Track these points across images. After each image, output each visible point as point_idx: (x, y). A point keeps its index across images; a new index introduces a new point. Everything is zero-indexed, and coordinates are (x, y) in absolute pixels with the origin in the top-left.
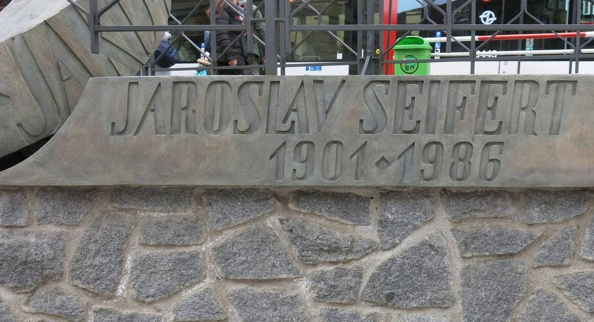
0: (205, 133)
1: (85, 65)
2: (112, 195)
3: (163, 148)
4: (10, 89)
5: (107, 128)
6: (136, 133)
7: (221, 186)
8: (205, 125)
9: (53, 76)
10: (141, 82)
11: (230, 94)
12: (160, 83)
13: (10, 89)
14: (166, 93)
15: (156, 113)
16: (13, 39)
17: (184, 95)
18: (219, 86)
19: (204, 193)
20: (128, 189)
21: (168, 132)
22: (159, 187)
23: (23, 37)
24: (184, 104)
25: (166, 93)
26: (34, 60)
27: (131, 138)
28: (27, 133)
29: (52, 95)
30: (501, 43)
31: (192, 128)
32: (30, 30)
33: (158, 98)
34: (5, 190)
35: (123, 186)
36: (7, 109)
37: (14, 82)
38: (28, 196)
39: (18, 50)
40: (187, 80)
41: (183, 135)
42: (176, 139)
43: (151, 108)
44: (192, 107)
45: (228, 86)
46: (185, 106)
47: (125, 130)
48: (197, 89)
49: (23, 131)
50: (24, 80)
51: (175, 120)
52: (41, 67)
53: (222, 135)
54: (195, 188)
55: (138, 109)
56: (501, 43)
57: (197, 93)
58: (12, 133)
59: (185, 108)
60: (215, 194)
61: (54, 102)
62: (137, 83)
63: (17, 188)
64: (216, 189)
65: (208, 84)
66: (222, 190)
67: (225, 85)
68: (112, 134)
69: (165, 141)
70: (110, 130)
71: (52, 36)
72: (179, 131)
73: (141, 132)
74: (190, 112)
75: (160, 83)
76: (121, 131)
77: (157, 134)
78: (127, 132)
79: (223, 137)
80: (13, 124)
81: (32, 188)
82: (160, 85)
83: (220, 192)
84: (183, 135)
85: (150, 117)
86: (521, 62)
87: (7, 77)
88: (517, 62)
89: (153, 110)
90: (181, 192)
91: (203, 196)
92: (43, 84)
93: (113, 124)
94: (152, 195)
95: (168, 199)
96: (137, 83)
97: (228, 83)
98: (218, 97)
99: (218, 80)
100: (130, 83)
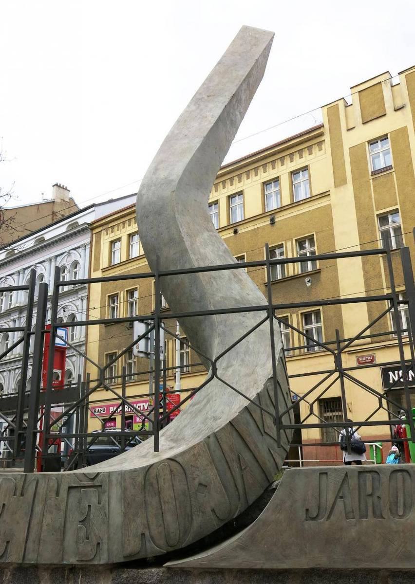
0: (392, 517)
1: (256, 455)
2: (303, 578)
3: (353, 532)
4: (208, 479)
5: (302, 514)
6: (329, 518)
7: (405, 569)
8: (390, 510)
9: (235, 466)
10: (330, 473)
11: (410, 481)
12: (347, 473)
13: (208, 479)
14: (353, 482)
15: (345, 500)
16: (209, 437)
17: (369, 484)
18: (399, 474)
19: (390, 576)
20: (318, 572)
21: (357, 517)
22: (346, 569)
23: (215, 435)
24: (369, 491)
25: (353, 482)
26: (223, 454)
27: (324, 523)
28: (218, 517)
29: (235, 483)
30: (392, 234)
31: (378, 513)
32: (220, 430)
33: (345, 486)
34: (207, 572)
35: (313, 569)
36: (205, 497)
37: (210, 473)
38: (227, 577)
39: (212, 446)
40: (371, 470)
41: (371, 520)
42: (364, 524)
43: (340, 496)
44: (378, 494)
45: (408, 474)
46: (370, 493)
47: (317, 516)
48: (380, 477)
49: (215, 516)
50: (216, 471)
51: (363, 506)
52: (228, 459)
53: (407, 519)
54: (380, 570)
55: (329, 497)
56: (392, 234)
57: (379, 481)
58: (208, 518)
59: (370, 495)
60: (400, 576)
61: (236, 489)
62: (326, 473)
63: (217, 570)
64: (400, 571)
65: (390, 472)
66: (407, 573)
67: (405, 473)
68: (306, 520)
69: (355, 525)
70: (305, 516)
71: (235, 434)
72: (366, 516)
73: (332, 518)
74: (376, 499)
75: (347, 473)
76: (315, 516)
77: (347, 518)
78: (319, 518)
79: (409, 521)
80: (209, 510)
81: (230, 570)
82: (346, 475)
83: (404, 574)
84: (371, 520)
85: (340, 503)
86: (289, 374)
87: (205, 469)
88: (290, 380)
89: (341, 497)
90: (367, 575)
91: (389, 579)
92: (229, 474)
93: (307, 510)
94: (340, 578)
95: (355, 581)
96: (326, 473)
97: (407, 472)
98: (400, 484)
99: (398, 469)
100: (320, 474)
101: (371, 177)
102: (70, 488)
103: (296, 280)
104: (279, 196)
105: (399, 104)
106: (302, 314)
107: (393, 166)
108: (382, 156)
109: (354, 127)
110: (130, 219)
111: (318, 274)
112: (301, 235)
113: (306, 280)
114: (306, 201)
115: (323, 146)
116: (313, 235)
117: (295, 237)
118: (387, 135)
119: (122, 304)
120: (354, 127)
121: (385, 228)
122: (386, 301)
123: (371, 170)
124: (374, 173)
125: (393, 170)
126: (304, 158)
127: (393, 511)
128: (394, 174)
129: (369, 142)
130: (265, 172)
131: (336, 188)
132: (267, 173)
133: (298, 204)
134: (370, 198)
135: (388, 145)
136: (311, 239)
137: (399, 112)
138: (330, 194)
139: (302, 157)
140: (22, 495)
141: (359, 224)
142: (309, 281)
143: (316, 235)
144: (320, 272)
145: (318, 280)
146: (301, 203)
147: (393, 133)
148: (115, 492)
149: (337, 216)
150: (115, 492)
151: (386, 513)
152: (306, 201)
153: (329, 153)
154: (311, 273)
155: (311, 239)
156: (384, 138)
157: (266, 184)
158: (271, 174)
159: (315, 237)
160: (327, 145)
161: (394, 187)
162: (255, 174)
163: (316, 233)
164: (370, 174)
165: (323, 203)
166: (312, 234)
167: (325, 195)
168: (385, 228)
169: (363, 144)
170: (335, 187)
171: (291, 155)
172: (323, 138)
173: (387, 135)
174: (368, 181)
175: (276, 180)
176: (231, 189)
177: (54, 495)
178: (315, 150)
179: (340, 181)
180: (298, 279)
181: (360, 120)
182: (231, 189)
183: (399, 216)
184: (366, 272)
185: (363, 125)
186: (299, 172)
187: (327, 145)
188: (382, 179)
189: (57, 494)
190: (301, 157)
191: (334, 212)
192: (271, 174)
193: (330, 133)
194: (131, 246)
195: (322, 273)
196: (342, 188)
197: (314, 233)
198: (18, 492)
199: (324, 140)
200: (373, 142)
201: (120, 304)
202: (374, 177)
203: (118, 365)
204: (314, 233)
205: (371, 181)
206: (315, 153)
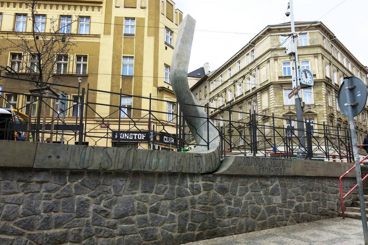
101: (123, 36)
102: (195, 156)
103: (72, 77)
104: (25, 25)
105: (143, 5)
106: (73, 96)
107: (135, 35)
108: (129, 28)
109: (119, 7)
110: (22, 3)
111: (86, 77)
112: (80, 53)
113: (79, 78)
114: (85, 36)
115: (101, 9)
116: (87, 55)
117: (77, 53)
118: (135, 18)
119: (71, 63)
120: (119, 7)
121: (79, 62)
122: (52, 99)
123: (124, 33)
124: (125, 35)
125: (135, 37)
126: (16, 8)
127: (251, 165)
128: (135, 39)
129: (125, 18)
130: (63, 9)
131: (104, 35)
132: (46, 10)
133: (81, 35)
134: (121, 47)
135: (134, 23)
136: (85, 58)
137: (142, 10)
138: (100, 37)
139: (46, 9)
140: (185, 157)
141: (113, 58)
142: (80, 80)
143: (89, 56)
144: (87, 76)
145: (86, 81)
146: (83, 35)
147: (138, 19)
148: (204, 158)
149: (102, 49)
150: (204, 158)
151: (250, 165)
152: (85, 36)
153: (104, 14)
154: (81, 75)
155: (85, 58)
156: (133, 19)
157: (17, 15)
158: (66, 12)
159: (88, 56)
160: (103, 9)
161: (134, 45)
162: (56, 8)
163: (89, 55)
164: (123, 34)
165: (96, 40)
166: (87, 54)
167: (97, 36)
168: (79, 62)
169: (122, 17)
170: (104, 34)
171: (87, 7)
172: (101, 5)
173: (135, 18)
174: (121, 38)
175: (69, 17)
176: (84, 13)
177: (192, 158)
178: (96, 9)
179: (107, 32)
180: (74, 77)
181: (123, 5)
182: (84, 13)
183: (133, 59)
184: (112, 83)
185: (124, 8)
186: (84, 18)
187: (103, 9)
188: (128, 39)
189: (192, 157)
190: (63, 9)
191: (101, 47)
192: (66, 12)
193: (106, 4)
194: (16, 22)
195: (89, 77)
196: (107, 36)
197: (88, 55)
198: (184, 156)
199: (102, 7)
200: (127, 19)
201: (69, 63)
202: (125, 37)
203: (18, 103)
204: (88, 55)
205: (123, 38)
206: (90, 11)
